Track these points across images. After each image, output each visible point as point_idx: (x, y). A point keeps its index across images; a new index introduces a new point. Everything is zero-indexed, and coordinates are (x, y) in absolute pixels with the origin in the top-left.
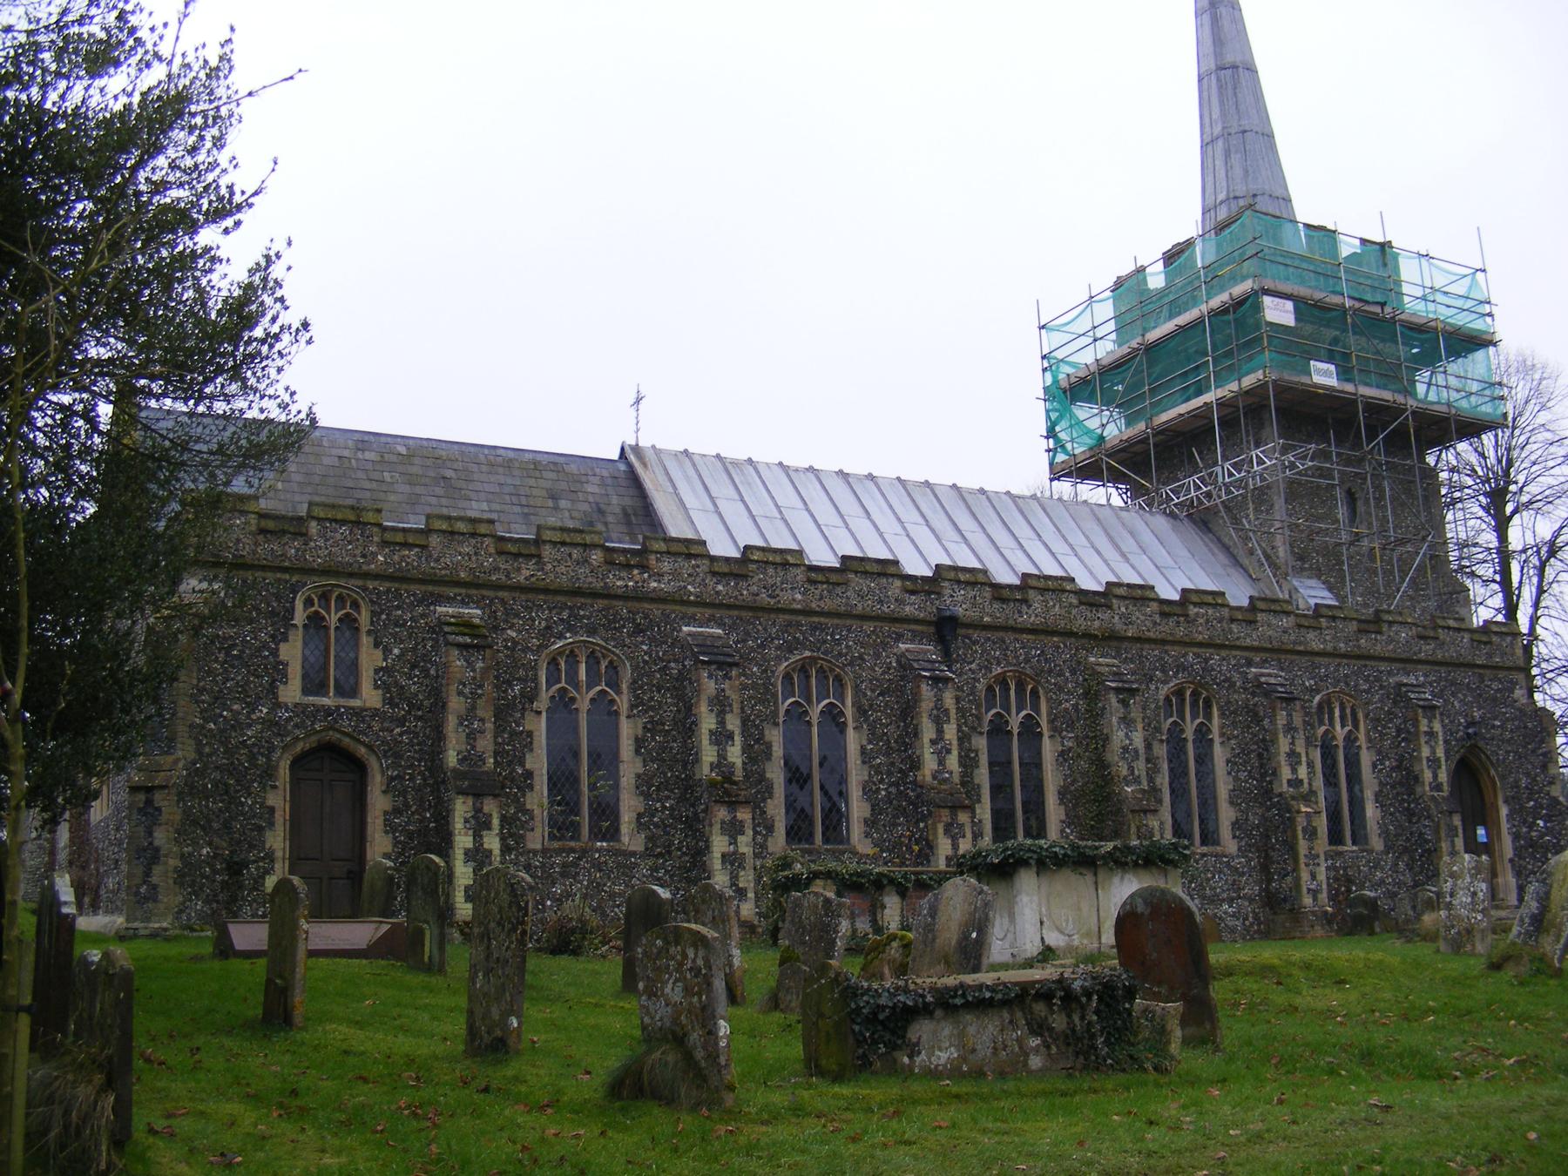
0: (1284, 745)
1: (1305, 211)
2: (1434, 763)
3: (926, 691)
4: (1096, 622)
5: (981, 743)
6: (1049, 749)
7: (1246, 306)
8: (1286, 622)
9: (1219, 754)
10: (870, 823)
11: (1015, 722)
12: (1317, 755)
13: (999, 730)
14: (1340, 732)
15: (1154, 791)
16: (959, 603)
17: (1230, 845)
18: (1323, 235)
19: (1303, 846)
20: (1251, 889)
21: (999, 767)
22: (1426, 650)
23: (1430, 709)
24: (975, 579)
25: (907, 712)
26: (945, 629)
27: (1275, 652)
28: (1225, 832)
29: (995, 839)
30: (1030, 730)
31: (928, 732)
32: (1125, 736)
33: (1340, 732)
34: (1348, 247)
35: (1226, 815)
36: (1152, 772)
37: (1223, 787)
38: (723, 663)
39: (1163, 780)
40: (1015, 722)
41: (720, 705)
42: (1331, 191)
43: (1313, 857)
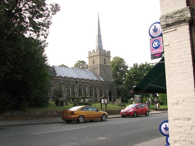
0: (97, 90)
1: (104, 49)
2: (107, 92)
3: (75, 86)
4: (85, 82)
5: (78, 89)
6: (82, 90)
7: (160, 42)
8: (98, 82)
9: (93, 90)
10: (71, 94)
11: (80, 88)
12: (100, 91)
13: (79, 89)
14: (101, 89)
15: (89, 93)
16: (77, 80)
17: (93, 96)
18: (105, 51)
19: (98, 97)
20: (94, 99)
21: (79, 91)
22: (108, 84)
23: (107, 88)
24: (78, 79)
25: (74, 87)
26: (76, 82)
27: (97, 84)
28: (93, 95)
29: (53, 94)
30: (81, 89)
31: (75, 89)
32: (87, 89)
33: (101, 89)
34: (107, 51)
35: (93, 94)
36: (77, 91)
37: (93, 92)
38: (63, 84)
39: (89, 92)
40: (80, 88)
41: (63, 87)
42: (106, 48)
43: (99, 98)
